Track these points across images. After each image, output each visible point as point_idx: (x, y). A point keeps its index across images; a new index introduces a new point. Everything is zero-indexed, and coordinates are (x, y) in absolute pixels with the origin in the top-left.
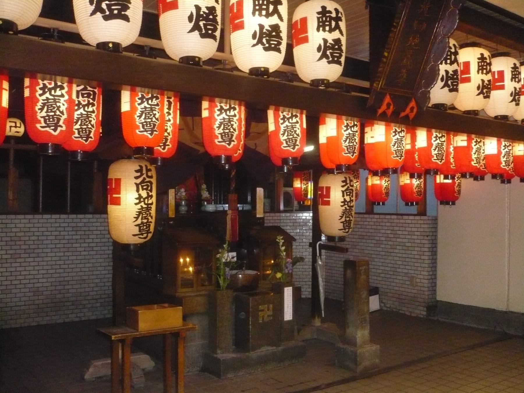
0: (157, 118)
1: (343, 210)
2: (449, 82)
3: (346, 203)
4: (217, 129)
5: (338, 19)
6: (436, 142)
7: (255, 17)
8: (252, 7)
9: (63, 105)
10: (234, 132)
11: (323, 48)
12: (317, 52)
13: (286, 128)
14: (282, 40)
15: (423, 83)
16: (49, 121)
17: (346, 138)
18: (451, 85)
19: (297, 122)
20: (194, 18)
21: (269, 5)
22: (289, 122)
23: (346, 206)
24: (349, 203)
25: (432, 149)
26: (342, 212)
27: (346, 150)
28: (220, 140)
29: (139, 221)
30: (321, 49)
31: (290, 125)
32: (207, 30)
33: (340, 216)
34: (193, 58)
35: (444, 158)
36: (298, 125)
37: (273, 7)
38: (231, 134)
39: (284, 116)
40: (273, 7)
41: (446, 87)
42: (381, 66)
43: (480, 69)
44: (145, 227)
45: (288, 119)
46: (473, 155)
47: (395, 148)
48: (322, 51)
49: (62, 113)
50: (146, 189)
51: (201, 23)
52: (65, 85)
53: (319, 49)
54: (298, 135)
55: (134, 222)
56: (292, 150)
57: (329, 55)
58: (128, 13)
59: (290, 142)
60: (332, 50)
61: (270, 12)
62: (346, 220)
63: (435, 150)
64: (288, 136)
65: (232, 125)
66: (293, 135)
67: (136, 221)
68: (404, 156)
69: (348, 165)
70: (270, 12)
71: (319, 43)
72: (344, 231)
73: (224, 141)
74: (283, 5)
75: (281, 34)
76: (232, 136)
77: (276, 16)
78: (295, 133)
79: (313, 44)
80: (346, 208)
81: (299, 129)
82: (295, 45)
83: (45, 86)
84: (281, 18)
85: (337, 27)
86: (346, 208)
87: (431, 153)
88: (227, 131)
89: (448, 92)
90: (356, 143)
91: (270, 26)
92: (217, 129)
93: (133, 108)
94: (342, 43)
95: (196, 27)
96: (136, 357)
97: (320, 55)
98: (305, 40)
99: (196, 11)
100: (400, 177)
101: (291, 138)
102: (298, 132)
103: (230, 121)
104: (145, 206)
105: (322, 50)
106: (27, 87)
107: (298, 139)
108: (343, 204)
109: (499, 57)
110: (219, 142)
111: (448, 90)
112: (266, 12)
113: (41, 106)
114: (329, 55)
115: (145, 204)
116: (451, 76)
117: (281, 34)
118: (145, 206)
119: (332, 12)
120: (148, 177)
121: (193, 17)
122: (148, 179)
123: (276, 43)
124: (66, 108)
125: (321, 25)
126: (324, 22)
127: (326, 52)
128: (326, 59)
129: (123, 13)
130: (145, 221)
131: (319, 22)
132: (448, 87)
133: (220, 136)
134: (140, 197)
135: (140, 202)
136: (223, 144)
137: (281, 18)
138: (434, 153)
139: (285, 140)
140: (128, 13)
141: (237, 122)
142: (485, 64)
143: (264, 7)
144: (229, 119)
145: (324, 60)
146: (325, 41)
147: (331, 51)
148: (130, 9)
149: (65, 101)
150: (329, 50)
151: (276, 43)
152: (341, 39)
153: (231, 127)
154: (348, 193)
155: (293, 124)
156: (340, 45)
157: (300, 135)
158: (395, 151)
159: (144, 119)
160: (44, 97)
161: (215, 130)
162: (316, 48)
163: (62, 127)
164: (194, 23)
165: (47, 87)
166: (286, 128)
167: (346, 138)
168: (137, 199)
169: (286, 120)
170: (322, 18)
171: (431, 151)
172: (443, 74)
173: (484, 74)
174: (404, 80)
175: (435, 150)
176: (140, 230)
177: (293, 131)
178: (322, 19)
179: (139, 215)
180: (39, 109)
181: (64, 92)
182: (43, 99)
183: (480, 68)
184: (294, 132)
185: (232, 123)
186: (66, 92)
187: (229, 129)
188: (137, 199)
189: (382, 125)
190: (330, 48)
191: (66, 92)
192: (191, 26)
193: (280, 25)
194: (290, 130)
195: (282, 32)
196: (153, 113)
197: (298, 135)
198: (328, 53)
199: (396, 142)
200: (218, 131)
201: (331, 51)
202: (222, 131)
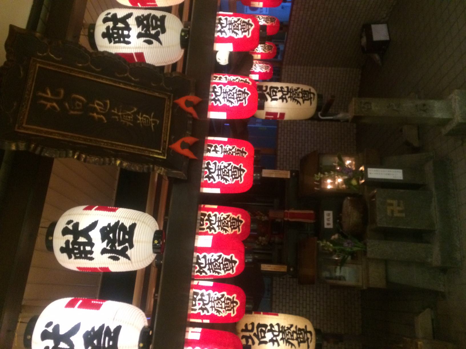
0: (227, 165)
1: (291, 100)
2: (153, 32)
3: (284, 97)
4: (227, 232)
5: (114, 18)
6: (217, 229)
7: (131, 41)
8: (83, 260)
9: (222, 215)
10: (230, 217)
11: (148, 39)
12: (119, 261)
13: (220, 227)
14: (150, 14)
15: (155, 85)
16: (235, 225)
17: (223, 230)
18: (157, 30)
19: (226, 19)
20: (113, 255)
21: (59, 347)
22: (215, 224)
23: (287, 96)
24: (285, 93)
25: (236, 37)
26: (293, 101)
27: (241, 102)
28: (237, 230)
29: (301, 100)
30: (114, 256)
31: (217, 223)
32: (124, 241)
33: (297, 104)
34: (182, 38)
35: (246, 20)
36: (229, 19)
37: (119, 24)
38: (234, 169)
39: (207, 228)
40: (119, 24)
41: (159, 37)
42: (133, 169)
43: (124, 39)
44: (306, 96)
45: (211, 224)
46: (233, 105)
47: (230, 230)
48: (152, 39)
49: (228, 216)
50: (276, 92)
51: (153, 32)
52: (207, 213)
53: (150, 43)
54: (239, 20)
55: (295, 347)
56: (245, 173)
57: (122, 246)
58: (127, 225)
59: (236, 175)
60: (116, 243)
61: (87, 241)
62: (302, 98)
63: (237, 34)
64: (228, 227)
65: (224, 218)
66: (228, 221)
67: (294, 346)
68: (246, 79)
69: (254, 155)
70: (87, 241)
71: (108, 259)
72: (312, 100)
73: (238, 226)
74: (116, 13)
75: (145, 15)
76: (234, 219)
77: (90, 233)
78: (231, 91)
79: (145, 48)
80: (289, 97)
81: (233, 18)
82: (156, 6)
83: (201, 308)
84: (129, 15)
85: (124, 20)
86: (289, 97)
87: (241, 39)
88: (229, 223)
89: (165, 34)
90: (237, 79)
91: (103, 241)
92: (227, 232)
93: (223, 108)
94: (140, 15)
95: (156, 37)
96: (402, 227)
97: (156, 41)
98: (140, 56)
99: (107, 253)
100: (265, 101)
101: (231, 224)
102: (235, 19)
103: (231, 24)
104: (289, 95)
105: (150, 39)
106: (202, 321)
107: (243, 19)
108: (285, 101)
109: (55, 254)
110: (239, 231)
111: (163, 35)
112: (126, 30)
113: (223, 231)
114: (122, 246)
115: (287, 94)
116: (145, 29)
117: (145, 15)
118: (289, 95)
119: (107, 25)
120: (252, 330)
121: (114, 256)
122: (255, 331)
123: (107, 338)
124: (225, 213)
125: (122, 39)
126: (81, 253)
127: (118, 250)
128: (127, 250)
129: (128, 230)
130: (301, 95)
131: (119, 42)
132: (159, 35)
133: (234, 230)
134: (272, 340)
135: (285, 98)
136: (240, 227)
137: (129, 15)
138: (240, 35)
139: (232, 229)
140: (127, 225)
141: (221, 214)
142: (115, 31)
143: (82, 248)
144: (219, 221)
145: (129, 252)
146: (104, 251)
147: (117, 244)
148: (123, 222)
149: (219, 214)
150: (115, 247)
151: (107, 338)
152: (137, 16)
153: (220, 300)
154: (274, 94)
155: (217, 220)
156: (142, 17)
157: (239, 18)
158: (238, 101)
159: (229, 177)
160: (217, 229)
161: (228, 234)
162: (149, 45)
163: (241, 166)
164: (153, 39)
165: (209, 226)
166: (220, 227)
167: (223, 230)
168: (273, 344)
169: (211, 227)
170: (115, 38)
171: (238, 39)
172: (143, 40)
173: (130, 34)
174: (153, 124)
175: (237, 34)
176: (308, 100)
177: (223, 221)
178: (116, 38)
179: (296, 100)
180: (226, 232)
181: (212, 214)
182: (218, 229)
183: (122, 39)
184: (225, 220)
185: (222, 219)
186: (213, 213)
187: (238, 24)
188: (273, 344)
189: (210, 114)
190: (113, 246)
191: (213, 213)
192: (127, 225)
193: (101, 227)
194: (234, 28)
195: (143, 14)
196: (234, 23)
197: (239, 20)
198: (119, 248)
199: (215, 310)
200: (229, 231)
201: (117, 244)
202: (236, 100)
